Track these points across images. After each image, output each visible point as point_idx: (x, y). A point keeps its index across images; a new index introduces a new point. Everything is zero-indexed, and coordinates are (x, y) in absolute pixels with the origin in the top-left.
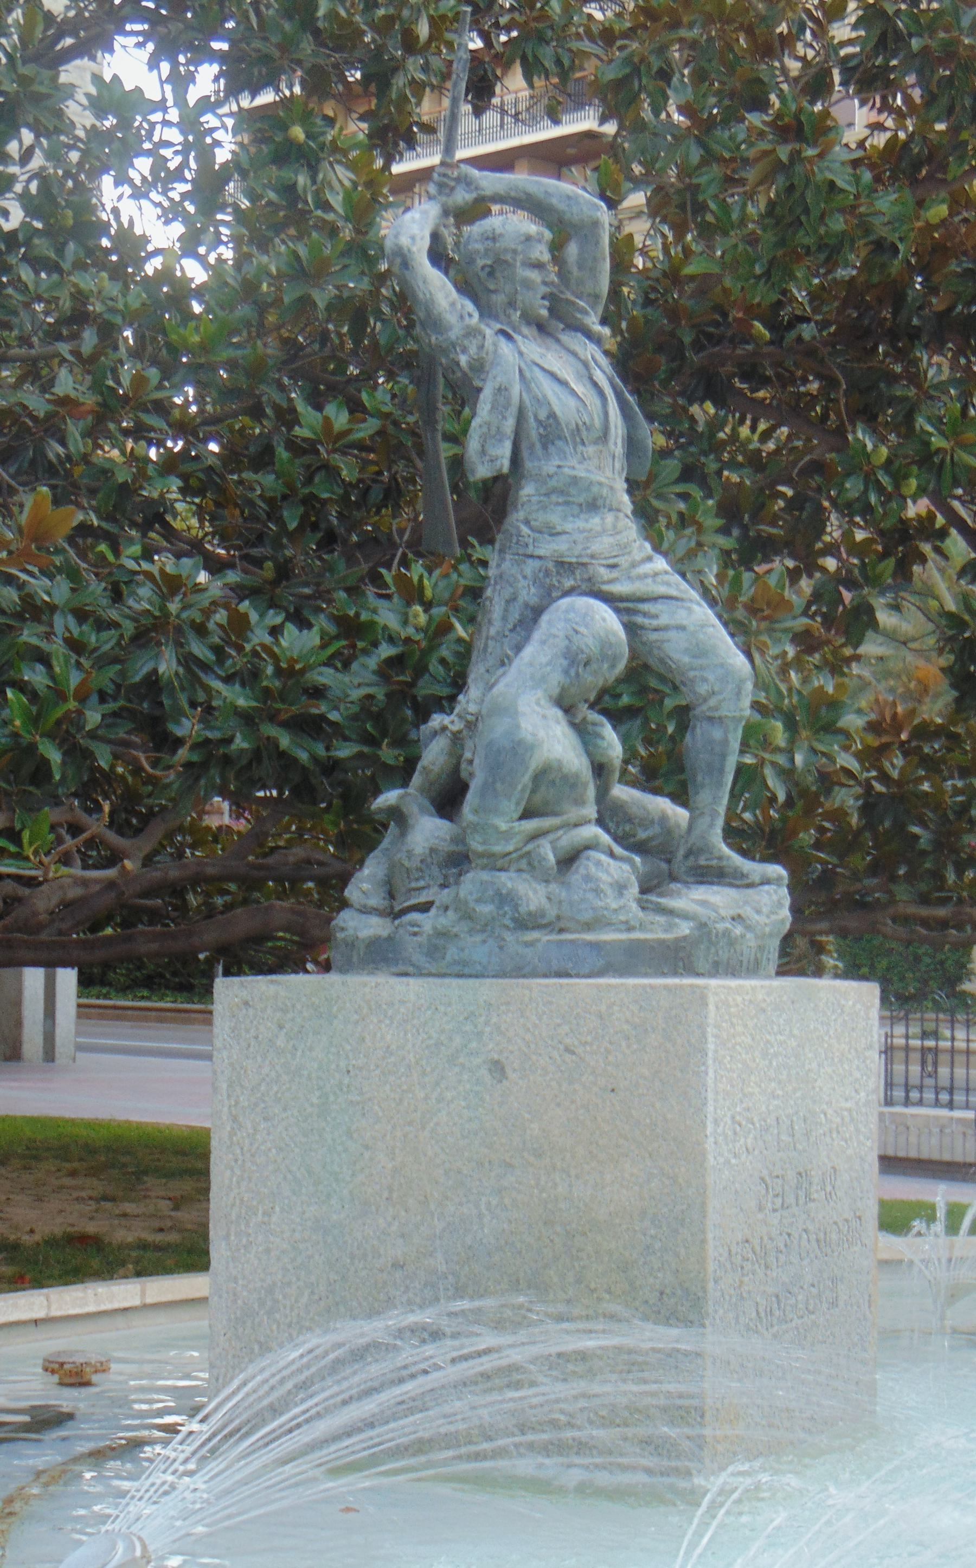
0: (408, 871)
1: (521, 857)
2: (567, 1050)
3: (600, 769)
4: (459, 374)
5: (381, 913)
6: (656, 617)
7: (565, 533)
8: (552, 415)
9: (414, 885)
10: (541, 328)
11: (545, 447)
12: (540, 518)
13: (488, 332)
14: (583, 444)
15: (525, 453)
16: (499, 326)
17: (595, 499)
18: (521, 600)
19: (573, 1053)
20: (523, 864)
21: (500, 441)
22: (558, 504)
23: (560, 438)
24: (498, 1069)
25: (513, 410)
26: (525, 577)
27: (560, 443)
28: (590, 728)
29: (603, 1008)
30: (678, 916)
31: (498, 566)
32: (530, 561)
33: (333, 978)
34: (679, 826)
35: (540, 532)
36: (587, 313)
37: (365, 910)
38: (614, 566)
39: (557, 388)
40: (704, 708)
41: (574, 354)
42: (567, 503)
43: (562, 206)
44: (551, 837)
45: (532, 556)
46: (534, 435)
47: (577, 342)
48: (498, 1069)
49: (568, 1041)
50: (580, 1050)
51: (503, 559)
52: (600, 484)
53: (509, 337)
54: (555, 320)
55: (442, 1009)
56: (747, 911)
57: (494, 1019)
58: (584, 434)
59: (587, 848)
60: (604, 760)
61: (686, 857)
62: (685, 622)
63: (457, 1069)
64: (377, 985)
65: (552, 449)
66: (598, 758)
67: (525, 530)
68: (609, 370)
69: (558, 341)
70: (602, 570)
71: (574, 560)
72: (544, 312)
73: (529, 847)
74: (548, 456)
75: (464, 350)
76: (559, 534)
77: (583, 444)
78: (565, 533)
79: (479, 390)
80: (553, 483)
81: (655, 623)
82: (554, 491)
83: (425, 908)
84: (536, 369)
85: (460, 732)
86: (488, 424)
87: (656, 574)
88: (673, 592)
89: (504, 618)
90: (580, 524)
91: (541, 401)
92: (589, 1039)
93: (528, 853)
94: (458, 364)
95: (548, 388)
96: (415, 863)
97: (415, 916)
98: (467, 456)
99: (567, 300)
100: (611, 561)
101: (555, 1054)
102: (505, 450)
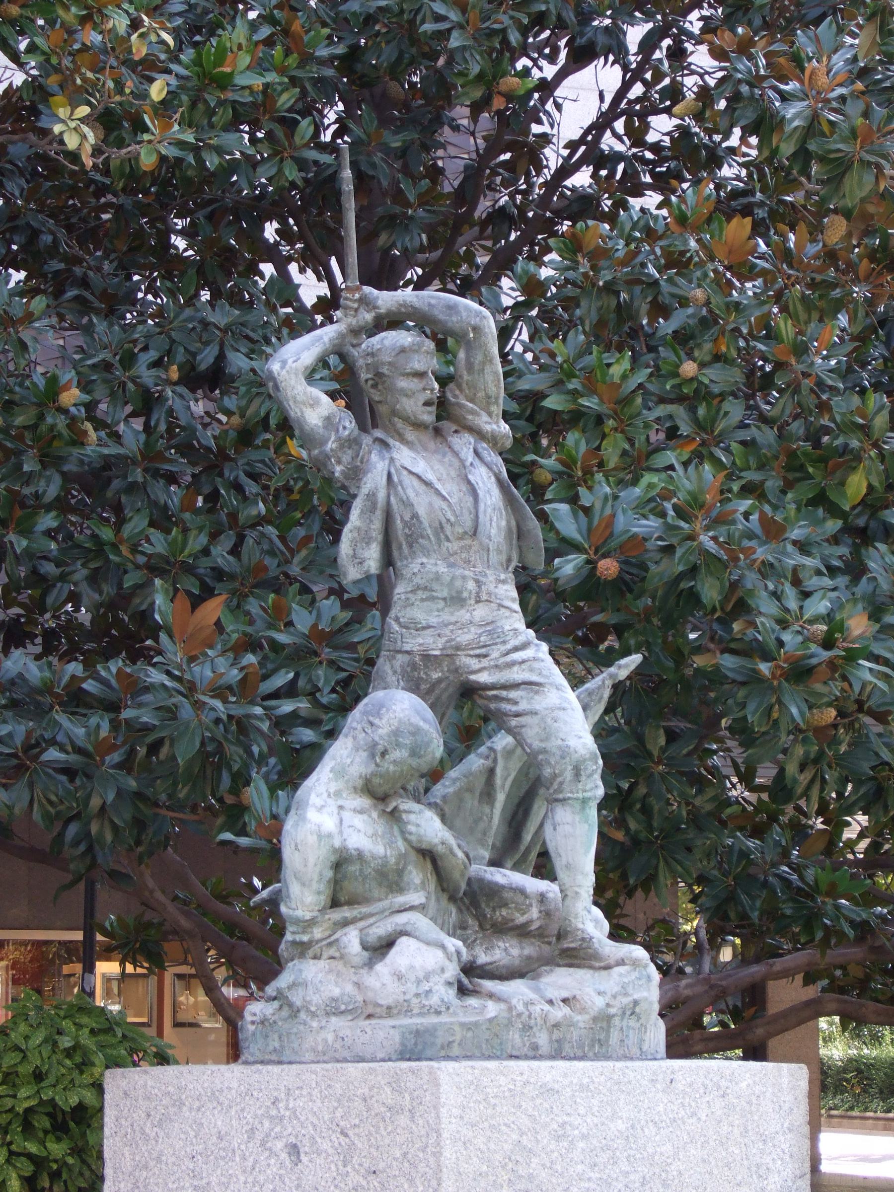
1: (330, 945)
7: (429, 627)
8: (415, 516)
11: (411, 546)
14: (448, 540)
15: (395, 554)
17: (460, 592)
19: (346, 1135)
20: (332, 952)
21: (368, 544)
22: (422, 600)
23: (423, 537)
24: (294, 1150)
28: (404, 816)
32: (399, 656)
33: (169, 1071)
35: (407, 628)
36: (478, 415)
38: (486, 656)
42: (433, 599)
43: (441, 317)
44: (361, 924)
45: (399, 652)
46: (402, 539)
48: (294, 1150)
50: (350, 1133)
52: (464, 578)
58: (448, 529)
62: (538, 707)
63: (267, 1153)
67: (396, 627)
70: (474, 664)
71: (437, 653)
74: (413, 554)
75: (339, 462)
76: (424, 628)
77: (448, 540)
78: (429, 627)
80: (417, 580)
81: (514, 708)
84: (405, 473)
86: (359, 529)
90: (446, 617)
91: (407, 504)
92: (357, 1121)
93: (337, 940)
100: (478, 652)
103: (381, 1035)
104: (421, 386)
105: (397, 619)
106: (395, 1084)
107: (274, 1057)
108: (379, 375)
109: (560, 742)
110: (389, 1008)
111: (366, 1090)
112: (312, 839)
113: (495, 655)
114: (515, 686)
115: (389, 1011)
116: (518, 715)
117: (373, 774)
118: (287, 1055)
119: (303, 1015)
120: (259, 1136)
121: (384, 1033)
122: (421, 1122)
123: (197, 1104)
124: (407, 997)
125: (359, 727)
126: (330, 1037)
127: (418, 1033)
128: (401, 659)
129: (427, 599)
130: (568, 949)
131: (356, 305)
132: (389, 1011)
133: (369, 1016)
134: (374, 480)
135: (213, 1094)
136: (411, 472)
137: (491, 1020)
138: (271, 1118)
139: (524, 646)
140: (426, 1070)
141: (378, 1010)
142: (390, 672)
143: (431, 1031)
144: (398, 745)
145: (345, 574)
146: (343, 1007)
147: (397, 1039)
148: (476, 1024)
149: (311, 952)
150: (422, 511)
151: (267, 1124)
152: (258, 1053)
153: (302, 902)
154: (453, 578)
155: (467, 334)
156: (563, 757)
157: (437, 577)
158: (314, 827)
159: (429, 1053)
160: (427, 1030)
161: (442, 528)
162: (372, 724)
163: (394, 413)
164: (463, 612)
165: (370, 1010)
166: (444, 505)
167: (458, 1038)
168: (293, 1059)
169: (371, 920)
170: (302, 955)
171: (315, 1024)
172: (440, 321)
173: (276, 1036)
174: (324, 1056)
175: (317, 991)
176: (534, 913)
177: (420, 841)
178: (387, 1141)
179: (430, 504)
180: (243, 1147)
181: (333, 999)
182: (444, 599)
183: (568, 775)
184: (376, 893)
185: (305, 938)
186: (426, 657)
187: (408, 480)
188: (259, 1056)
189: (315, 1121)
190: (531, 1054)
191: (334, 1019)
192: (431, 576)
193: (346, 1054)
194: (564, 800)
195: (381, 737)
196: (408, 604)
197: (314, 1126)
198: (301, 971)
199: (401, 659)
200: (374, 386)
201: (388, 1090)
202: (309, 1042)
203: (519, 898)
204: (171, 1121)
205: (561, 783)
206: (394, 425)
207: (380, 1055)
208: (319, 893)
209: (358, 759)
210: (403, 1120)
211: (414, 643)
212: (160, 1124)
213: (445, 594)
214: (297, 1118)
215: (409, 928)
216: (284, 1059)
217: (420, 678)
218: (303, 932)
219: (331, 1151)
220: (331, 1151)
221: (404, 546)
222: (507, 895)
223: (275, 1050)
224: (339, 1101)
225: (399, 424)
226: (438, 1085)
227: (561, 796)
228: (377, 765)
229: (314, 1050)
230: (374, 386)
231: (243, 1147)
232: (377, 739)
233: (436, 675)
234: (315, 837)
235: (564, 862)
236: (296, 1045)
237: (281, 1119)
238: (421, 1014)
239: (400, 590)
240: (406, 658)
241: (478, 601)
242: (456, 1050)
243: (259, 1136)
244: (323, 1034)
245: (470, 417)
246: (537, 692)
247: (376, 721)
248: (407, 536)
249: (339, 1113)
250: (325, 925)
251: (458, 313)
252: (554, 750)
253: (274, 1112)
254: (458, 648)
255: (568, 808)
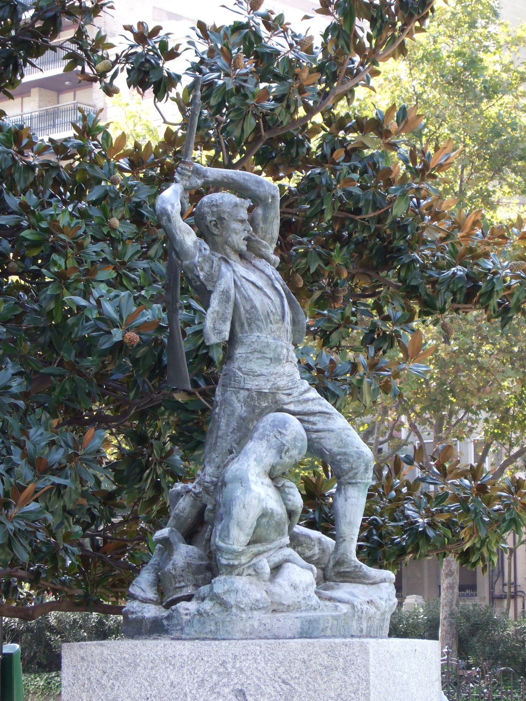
0: (174, 577)
1: (249, 567)
2: (284, 682)
3: (291, 514)
4: (198, 283)
5: (156, 603)
6: (314, 424)
7: (262, 375)
8: (254, 307)
9: (177, 585)
10: (242, 256)
11: (249, 325)
12: (247, 366)
13: (215, 259)
14: (271, 323)
15: (238, 329)
16: (220, 255)
18: (237, 414)
19: (287, 684)
20: (251, 571)
22: (258, 358)
23: (259, 320)
25: (231, 303)
26: (239, 401)
27: (260, 323)
28: (286, 490)
29: (306, 656)
30: (340, 601)
31: (223, 395)
32: (242, 391)
34: (328, 548)
35: (248, 375)
37: (145, 601)
38: (289, 395)
39: (256, 290)
40: (347, 477)
41: (263, 272)
42: (264, 358)
43: (253, 187)
44: (266, 555)
45: (243, 389)
46: (244, 320)
47: (261, 263)
49: (284, 677)
50: (292, 682)
51: (226, 391)
52: (282, 346)
53: (227, 262)
54: (250, 253)
55: (205, 659)
56: (375, 598)
57: (237, 666)
59: (287, 561)
60: (293, 508)
61: (335, 566)
62: (333, 427)
64: (165, 645)
65: (253, 325)
66: (290, 507)
68: (282, 282)
69: (251, 263)
70: (285, 397)
72: (244, 248)
73: (254, 561)
75: (202, 270)
76: (258, 375)
77: (271, 323)
78: (262, 375)
79: (210, 292)
80: (255, 346)
81: (315, 427)
82: (255, 351)
83: (189, 598)
84: (244, 280)
85: (200, 493)
86: (218, 312)
87: (314, 399)
88: (325, 410)
89: (227, 425)
90: (271, 370)
91: (248, 299)
92: (297, 675)
93: (254, 564)
94: (198, 277)
95: (251, 291)
96: (179, 571)
97: (183, 604)
98: (205, 331)
99: (256, 241)
100: (288, 392)
101: (276, 685)
102: (227, 328)
103: (290, 622)
104: (243, 228)
105: (240, 369)
106: (331, 652)
107: (209, 636)
108: (221, 219)
109: (356, 449)
110: (289, 606)
111: (306, 656)
112: (255, 502)
113: (296, 394)
114: (314, 414)
115: (288, 608)
116: (317, 431)
117: (277, 464)
118: (222, 634)
119: (234, 610)
120: (208, 685)
121: (290, 622)
122: (353, 675)
123: (151, 665)
124: (300, 600)
125: (272, 434)
126: (256, 624)
127: (310, 622)
128: (243, 394)
129: (260, 358)
130: (341, 573)
131: (190, 174)
132: (288, 608)
133: (274, 611)
134: (227, 280)
135: (167, 658)
136: (247, 280)
137: (345, 614)
138: (219, 674)
139: (306, 392)
140: (358, 645)
141: (281, 607)
142: (236, 401)
143: (316, 620)
144: (295, 447)
145: (208, 340)
146: (261, 605)
147: (299, 625)
148: (339, 616)
149: (236, 572)
150: (258, 304)
151: (215, 677)
152: (193, 633)
153: (238, 540)
154: (276, 347)
155: (268, 199)
156: (359, 458)
157: (268, 345)
158: (257, 495)
159: (316, 634)
160: (315, 620)
161: (269, 315)
162: (280, 433)
163: (226, 242)
164: (280, 367)
165: (275, 607)
166: (269, 302)
167: (330, 625)
168: (226, 637)
169: (271, 552)
170: (230, 573)
171: (244, 616)
172: (251, 190)
173: (213, 623)
174: (251, 635)
175: (246, 595)
176: (316, 550)
177: (293, 505)
178: (323, 687)
179: (262, 301)
180: (194, 692)
181: (257, 601)
182: (271, 359)
183: (362, 469)
184: (273, 536)
185: (236, 563)
186: (260, 393)
187: (247, 285)
188: (194, 634)
189: (259, 674)
190: (359, 634)
191: (255, 613)
192: (264, 344)
193: (267, 634)
194: (356, 483)
195: (287, 441)
196: (247, 360)
197: (259, 679)
198: (232, 583)
199: (243, 394)
200: (216, 225)
201: (325, 656)
202: (240, 626)
203: (309, 541)
204: (126, 675)
205: (356, 473)
206: (225, 250)
207: (289, 635)
208: (248, 535)
209: (270, 454)
210: (337, 674)
211: (253, 384)
212: (116, 678)
213: (271, 355)
214: (242, 673)
215: (291, 558)
216: (219, 637)
217: (255, 405)
218: (235, 559)
219: (273, 693)
220: (273, 693)
221: (246, 325)
222: (302, 539)
223: (211, 631)
224: (281, 663)
225: (228, 250)
226: (368, 653)
227: (353, 481)
228: (281, 458)
229: (243, 631)
230: (216, 225)
231: (194, 692)
232: (284, 442)
233: (264, 404)
234: (257, 501)
235: (348, 520)
236: (229, 629)
237: (229, 674)
238: (307, 610)
239: (240, 351)
240: (247, 393)
241: (287, 362)
242: (329, 632)
243: (208, 685)
244: (251, 622)
245: (263, 249)
246: (329, 418)
247: (284, 431)
248: (247, 318)
249: (281, 670)
250: (249, 555)
251: (263, 186)
252: (353, 454)
253: (221, 670)
254: (278, 389)
255: (356, 489)
